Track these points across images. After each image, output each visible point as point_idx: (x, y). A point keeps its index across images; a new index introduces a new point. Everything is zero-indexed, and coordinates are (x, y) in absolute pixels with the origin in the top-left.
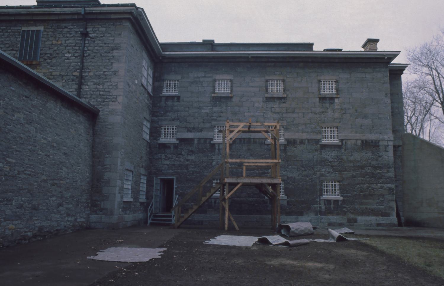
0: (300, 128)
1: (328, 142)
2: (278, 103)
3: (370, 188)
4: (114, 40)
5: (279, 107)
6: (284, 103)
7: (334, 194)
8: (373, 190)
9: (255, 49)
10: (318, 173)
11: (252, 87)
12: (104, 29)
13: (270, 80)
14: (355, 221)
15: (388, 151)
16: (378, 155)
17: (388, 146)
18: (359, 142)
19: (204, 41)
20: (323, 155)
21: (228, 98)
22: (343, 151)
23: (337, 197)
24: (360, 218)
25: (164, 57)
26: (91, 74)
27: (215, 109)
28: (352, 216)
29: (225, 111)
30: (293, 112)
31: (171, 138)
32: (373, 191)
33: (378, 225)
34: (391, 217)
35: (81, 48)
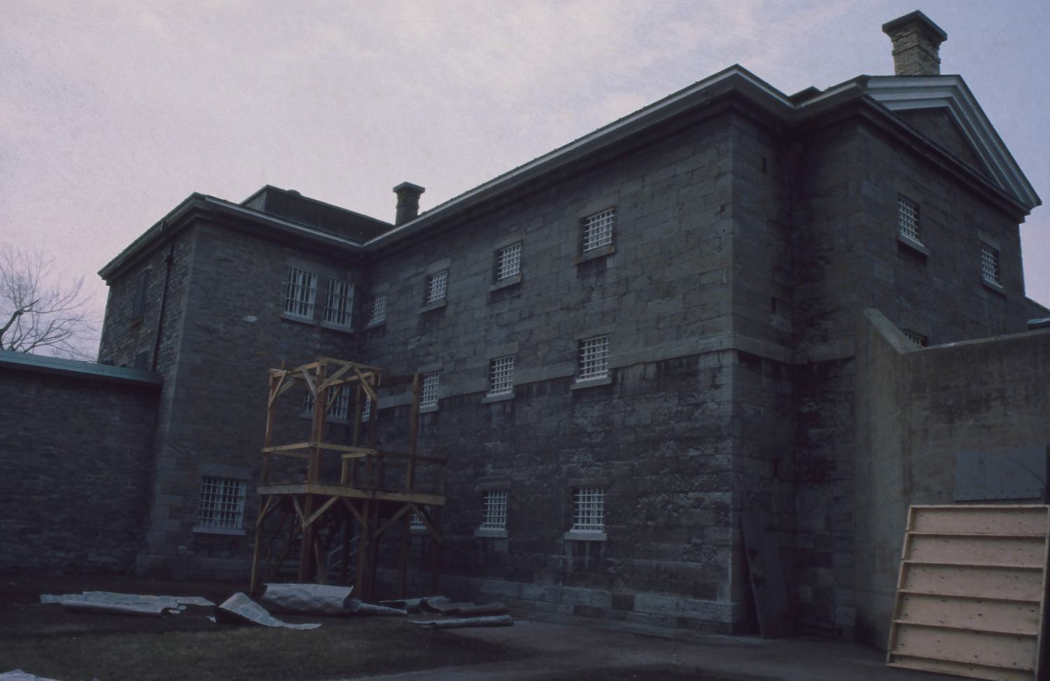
0: (540, 354)
3: (670, 507)
6: (518, 297)
8: (676, 511)
10: (565, 467)
11: (476, 274)
13: (504, 250)
14: (628, 604)
15: (717, 387)
16: (693, 401)
17: (720, 368)
18: (651, 370)
21: (440, 311)
22: (615, 401)
27: (424, 339)
28: (624, 590)
30: (531, 316)
33: (683, 622)
34: (719, 602)
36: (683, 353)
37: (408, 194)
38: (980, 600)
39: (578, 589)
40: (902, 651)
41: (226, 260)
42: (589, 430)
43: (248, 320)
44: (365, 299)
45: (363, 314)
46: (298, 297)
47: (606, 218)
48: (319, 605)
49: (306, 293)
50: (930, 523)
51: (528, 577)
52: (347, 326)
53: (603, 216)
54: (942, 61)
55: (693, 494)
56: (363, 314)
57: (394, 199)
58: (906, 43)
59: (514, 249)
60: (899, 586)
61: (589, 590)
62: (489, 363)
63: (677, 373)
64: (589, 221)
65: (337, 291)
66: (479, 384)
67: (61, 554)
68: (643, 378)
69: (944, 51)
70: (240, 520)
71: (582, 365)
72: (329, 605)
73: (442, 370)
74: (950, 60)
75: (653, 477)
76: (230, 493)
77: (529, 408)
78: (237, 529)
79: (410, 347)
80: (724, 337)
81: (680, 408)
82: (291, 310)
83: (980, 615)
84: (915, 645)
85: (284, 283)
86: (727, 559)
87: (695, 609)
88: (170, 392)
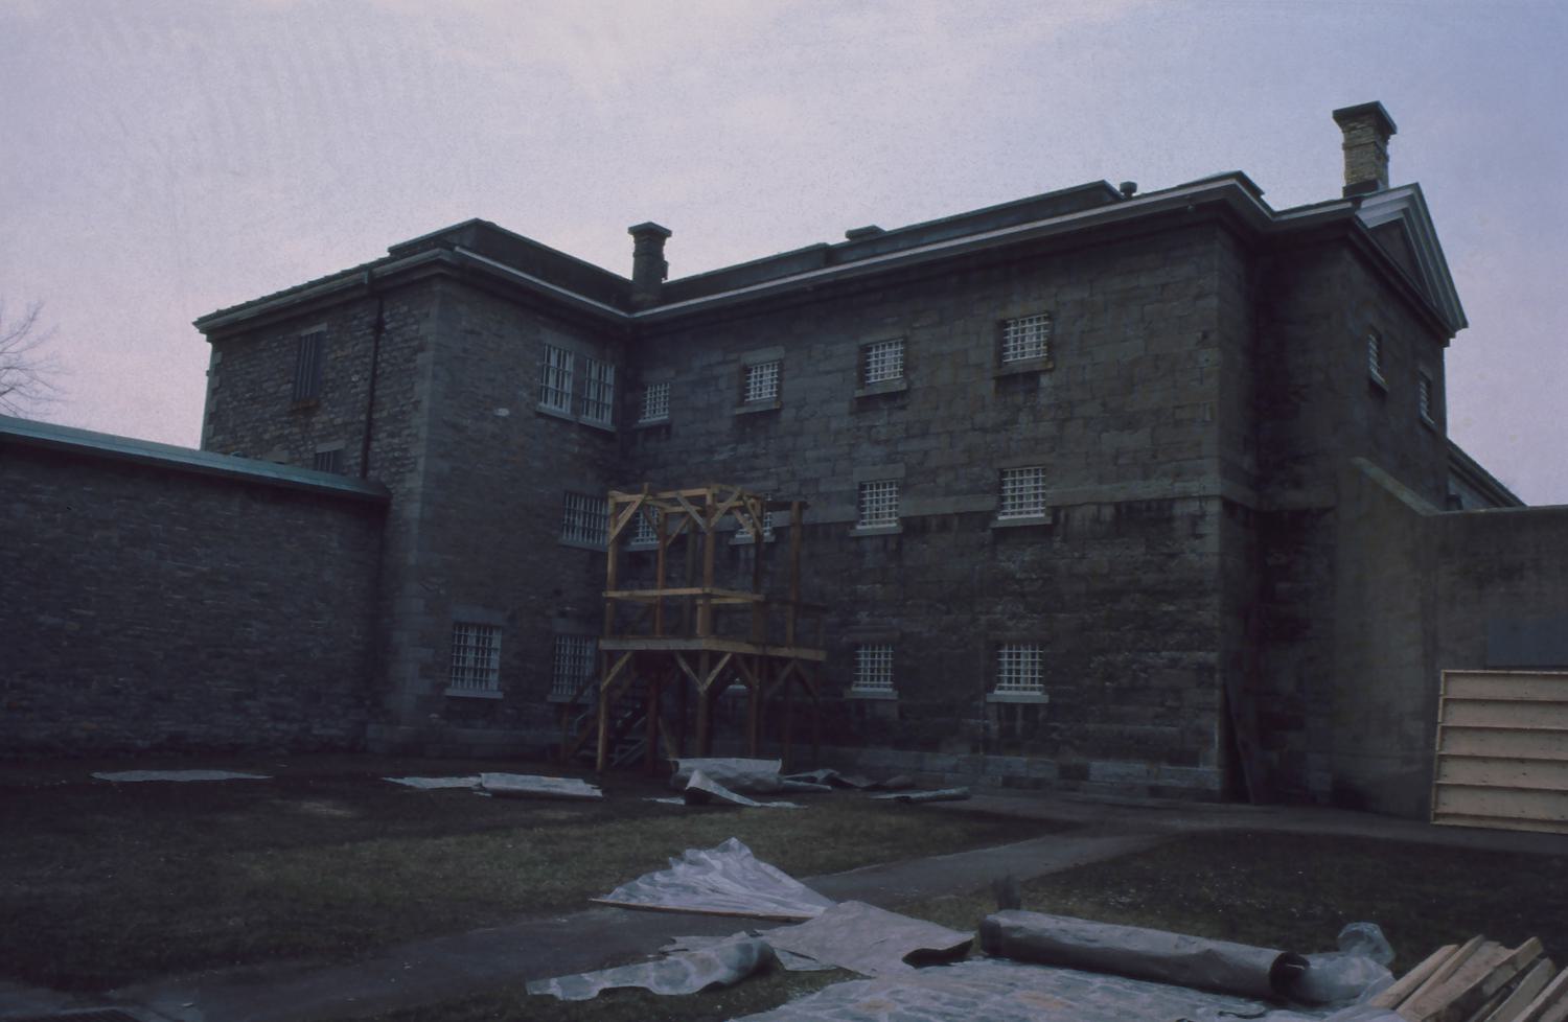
0: (941, 480)
1: (1013, 517)
2: (886, 413)
3: (1134, 667)
4: (418, 330)
5: (889, 423)
6: (903, 408)
7: (875, 682)
8: (1145, 671)
9: (935, 237)
10: (983, 619)
11: (828, 373)
12: (405, 308)
13: (874, 346)
14: (1083, 773)
15: (1200, 536)
16: (1165, 550)
17: (1203, 516)
18: (1108, 513)
19: (851, 234)
20: (1001, 561)
21: (771, 415)
22: (1057, 545)
23: (1037, 695)
24: (1099, 768)
25: (638, 325)
26: (385, 414)
27: (743, 449)
28: (1075, 759)
29: (764, 451)
30: (924, 434)
31: (874, 520)
32: (1143, 675)
33: (1155, 791)
34: (1201, 768)
35: (367, 360)
36: (1153, 496)
37: (650, 239)
38: (1522, 761)
39: (1007, 759)
40: (1442, 809)
41: (472, 332)
42: (1018, 576)
43: (499, 414)
44: (631, 387)
45: (628, 409)
46: (552, 384)
47: (1035, 324)
48: (748, 783)
49: (566, 383)
50: (1461, 688)
51: (932, 745)
52: (605, 421)
53: (1031, 321)
54: (1391, 159)
55: (1167, 653)
56: (628, 409)
57: (629, 243)
58: (1359, 137)
59: (890, 345)
60: (1437, 749)
61: (1025, 759)
62: (857, 488)
63: (1144, 520)
64: (1009, 325)
65: (594, 375)
66: (839, 512)
67: (283, 726)
68: (1097, 520)
69: (1394, 146)
70: (494, 678)
71: (1003, 499)
72: (759, 781)
73: (778, 490)
74: (1404, 164)
75: (1112, 634)
76: (484, 643)
77: (925, 546)
78: (492, 689)
79: (717, 457)
80: (1210, 482)
81: (1149, 557)
82: (546, 402)
83: (1524, 774)
84: (1454, 804)
85: (538, 364)
86: (1214, 725)
87: (1171, 776)
88: (411, 511)
